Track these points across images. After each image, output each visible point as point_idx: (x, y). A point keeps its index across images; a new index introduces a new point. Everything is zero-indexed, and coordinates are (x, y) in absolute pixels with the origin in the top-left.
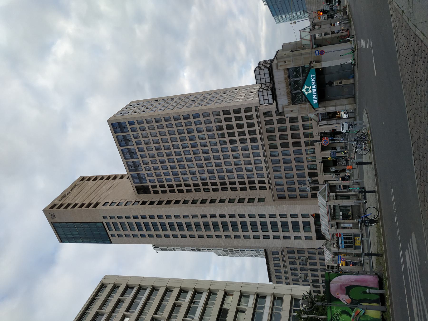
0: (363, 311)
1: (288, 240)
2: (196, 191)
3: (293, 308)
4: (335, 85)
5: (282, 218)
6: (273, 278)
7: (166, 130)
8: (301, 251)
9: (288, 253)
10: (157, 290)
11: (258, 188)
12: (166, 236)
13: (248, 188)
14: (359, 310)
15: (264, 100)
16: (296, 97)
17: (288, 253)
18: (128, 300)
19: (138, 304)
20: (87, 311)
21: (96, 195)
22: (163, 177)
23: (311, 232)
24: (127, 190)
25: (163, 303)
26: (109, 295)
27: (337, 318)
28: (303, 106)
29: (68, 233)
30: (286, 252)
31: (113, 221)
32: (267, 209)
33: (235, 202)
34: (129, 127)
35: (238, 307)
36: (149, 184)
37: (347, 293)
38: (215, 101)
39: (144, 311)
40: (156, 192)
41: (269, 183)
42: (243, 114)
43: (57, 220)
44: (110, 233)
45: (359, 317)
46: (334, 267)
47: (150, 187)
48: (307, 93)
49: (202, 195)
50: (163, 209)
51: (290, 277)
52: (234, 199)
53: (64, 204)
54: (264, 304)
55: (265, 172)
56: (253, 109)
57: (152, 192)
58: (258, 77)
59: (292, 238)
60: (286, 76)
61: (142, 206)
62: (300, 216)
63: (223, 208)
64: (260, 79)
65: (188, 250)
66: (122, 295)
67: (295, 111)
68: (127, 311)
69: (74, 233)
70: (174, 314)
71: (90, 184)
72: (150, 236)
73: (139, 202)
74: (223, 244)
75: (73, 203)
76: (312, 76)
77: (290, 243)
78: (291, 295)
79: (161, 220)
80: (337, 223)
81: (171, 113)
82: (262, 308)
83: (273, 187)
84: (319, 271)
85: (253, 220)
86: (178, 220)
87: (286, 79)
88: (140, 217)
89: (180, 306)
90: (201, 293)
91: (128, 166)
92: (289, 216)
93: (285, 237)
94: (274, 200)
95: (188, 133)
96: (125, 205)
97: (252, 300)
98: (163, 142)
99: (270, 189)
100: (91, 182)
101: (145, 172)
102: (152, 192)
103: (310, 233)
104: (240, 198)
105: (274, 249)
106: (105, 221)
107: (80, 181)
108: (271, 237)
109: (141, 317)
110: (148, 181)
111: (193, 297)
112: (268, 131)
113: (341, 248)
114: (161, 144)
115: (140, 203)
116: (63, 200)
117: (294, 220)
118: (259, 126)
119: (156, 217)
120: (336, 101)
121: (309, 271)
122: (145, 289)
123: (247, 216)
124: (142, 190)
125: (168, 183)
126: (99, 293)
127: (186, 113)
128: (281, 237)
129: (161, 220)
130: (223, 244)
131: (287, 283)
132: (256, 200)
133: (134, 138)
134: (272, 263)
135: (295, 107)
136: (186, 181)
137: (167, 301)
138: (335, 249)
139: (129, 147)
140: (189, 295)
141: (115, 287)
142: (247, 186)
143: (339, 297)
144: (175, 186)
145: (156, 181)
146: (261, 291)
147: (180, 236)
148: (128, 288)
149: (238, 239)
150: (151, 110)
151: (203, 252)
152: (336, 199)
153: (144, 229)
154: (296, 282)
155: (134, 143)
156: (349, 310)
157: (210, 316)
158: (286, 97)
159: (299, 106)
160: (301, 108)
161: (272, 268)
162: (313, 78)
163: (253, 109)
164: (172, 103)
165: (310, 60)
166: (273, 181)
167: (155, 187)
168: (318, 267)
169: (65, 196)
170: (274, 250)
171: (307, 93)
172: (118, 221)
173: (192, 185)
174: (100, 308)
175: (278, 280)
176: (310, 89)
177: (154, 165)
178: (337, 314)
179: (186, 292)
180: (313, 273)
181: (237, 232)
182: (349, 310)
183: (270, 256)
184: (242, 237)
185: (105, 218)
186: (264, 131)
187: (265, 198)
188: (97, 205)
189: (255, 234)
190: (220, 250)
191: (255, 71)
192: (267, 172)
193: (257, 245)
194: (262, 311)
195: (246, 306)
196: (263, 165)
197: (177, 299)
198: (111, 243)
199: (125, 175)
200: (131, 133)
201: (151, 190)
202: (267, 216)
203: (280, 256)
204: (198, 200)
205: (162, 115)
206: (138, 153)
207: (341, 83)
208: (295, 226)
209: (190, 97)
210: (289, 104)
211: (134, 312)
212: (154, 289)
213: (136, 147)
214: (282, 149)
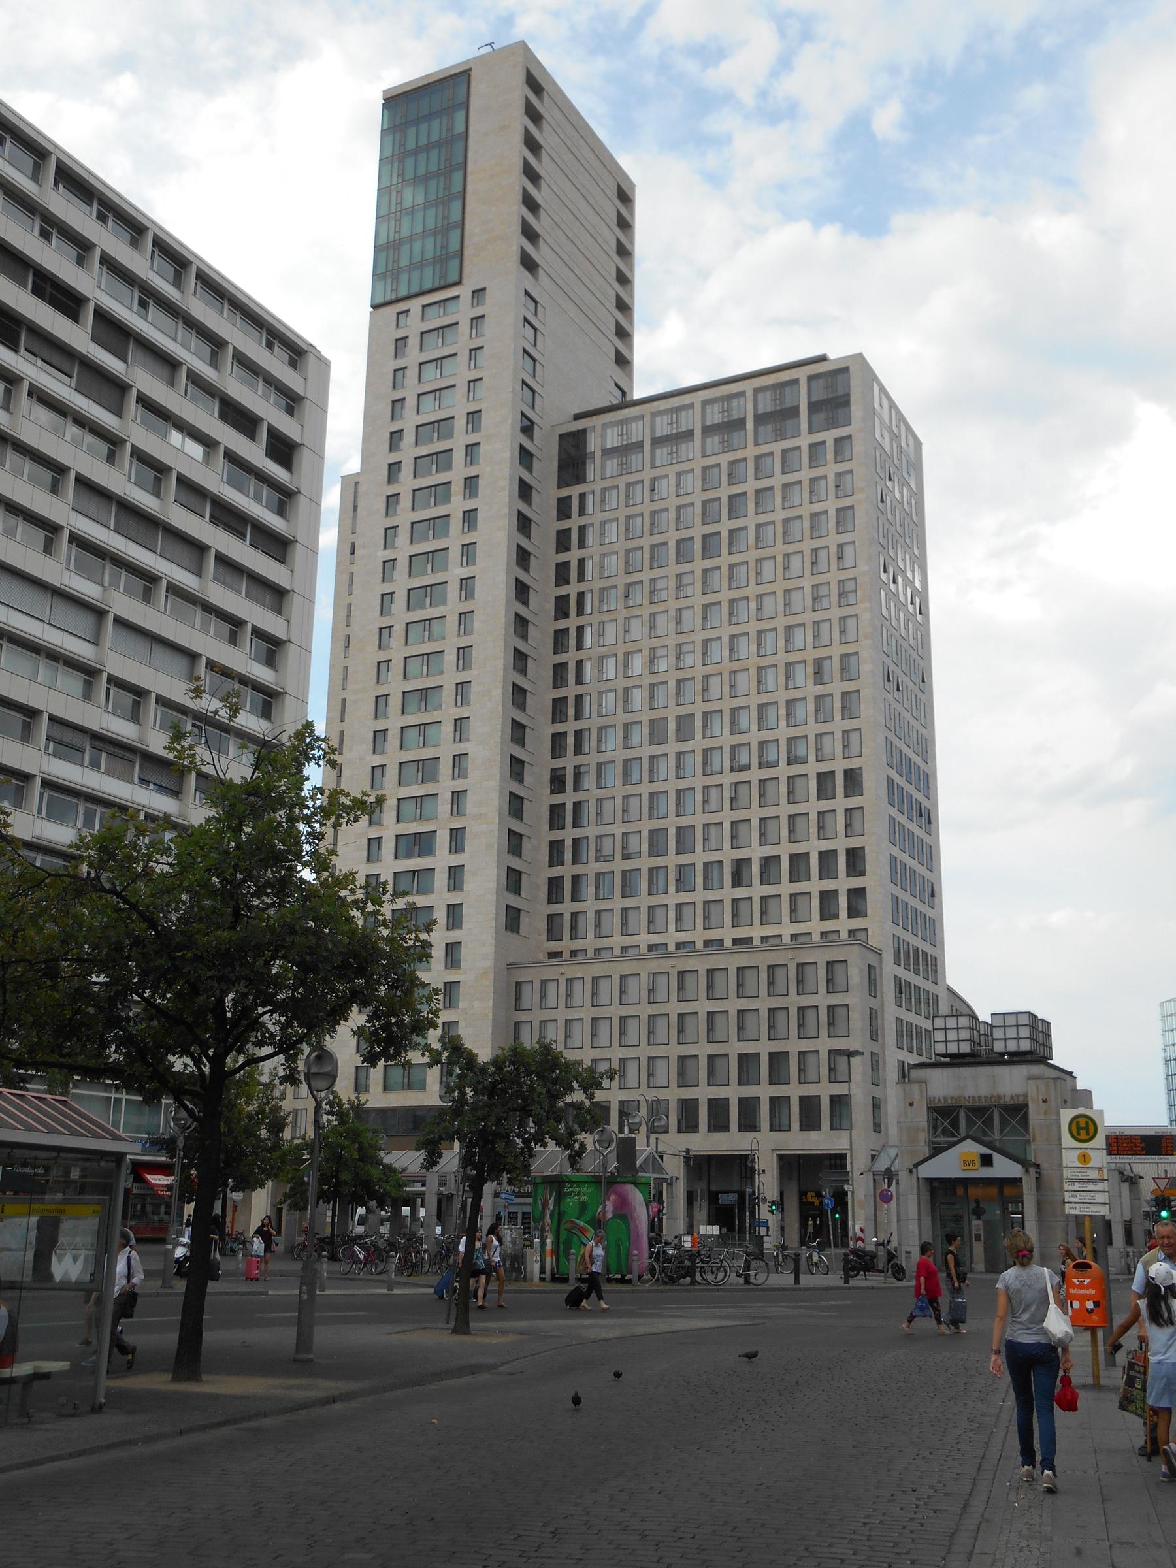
4: (974, 1222)
15: (946, 1029)
16: (948, 1121)
19: (239, 488)
21: (566, 258)
28: (923, 1136)
34: (829, 436)
44: (415, 305)
57: (565, 492)
58: (1011, 1021)
60: (1008, 1099)
71: (605, 230)
75: (543, 167)
83: (563, 969)
88: (472, 439)
94: (511, 967)
102: (565, 492)
103: (380, 1088)
104: (525, 840)
107: (620, 189)
123: (455, 860)
132: (514, 901)
133: (785, 452)
139: (750, 425)
140: (262, 674)
141: (292, 402)
155: (765, 449)
156: (588, 1216)
158: (956, 1094)
163: (856, 923)
165: (1045, 1166)
178: (579, 1194)
185: (478, 293)
191: (1029, 1013)
195: (40, 812)
198: (375, 307)
200: (804, 441)
201: (574, 491)
207: (978, 1238)
209: (918, 680)
210: (930, 1100)
213: (751, 452)
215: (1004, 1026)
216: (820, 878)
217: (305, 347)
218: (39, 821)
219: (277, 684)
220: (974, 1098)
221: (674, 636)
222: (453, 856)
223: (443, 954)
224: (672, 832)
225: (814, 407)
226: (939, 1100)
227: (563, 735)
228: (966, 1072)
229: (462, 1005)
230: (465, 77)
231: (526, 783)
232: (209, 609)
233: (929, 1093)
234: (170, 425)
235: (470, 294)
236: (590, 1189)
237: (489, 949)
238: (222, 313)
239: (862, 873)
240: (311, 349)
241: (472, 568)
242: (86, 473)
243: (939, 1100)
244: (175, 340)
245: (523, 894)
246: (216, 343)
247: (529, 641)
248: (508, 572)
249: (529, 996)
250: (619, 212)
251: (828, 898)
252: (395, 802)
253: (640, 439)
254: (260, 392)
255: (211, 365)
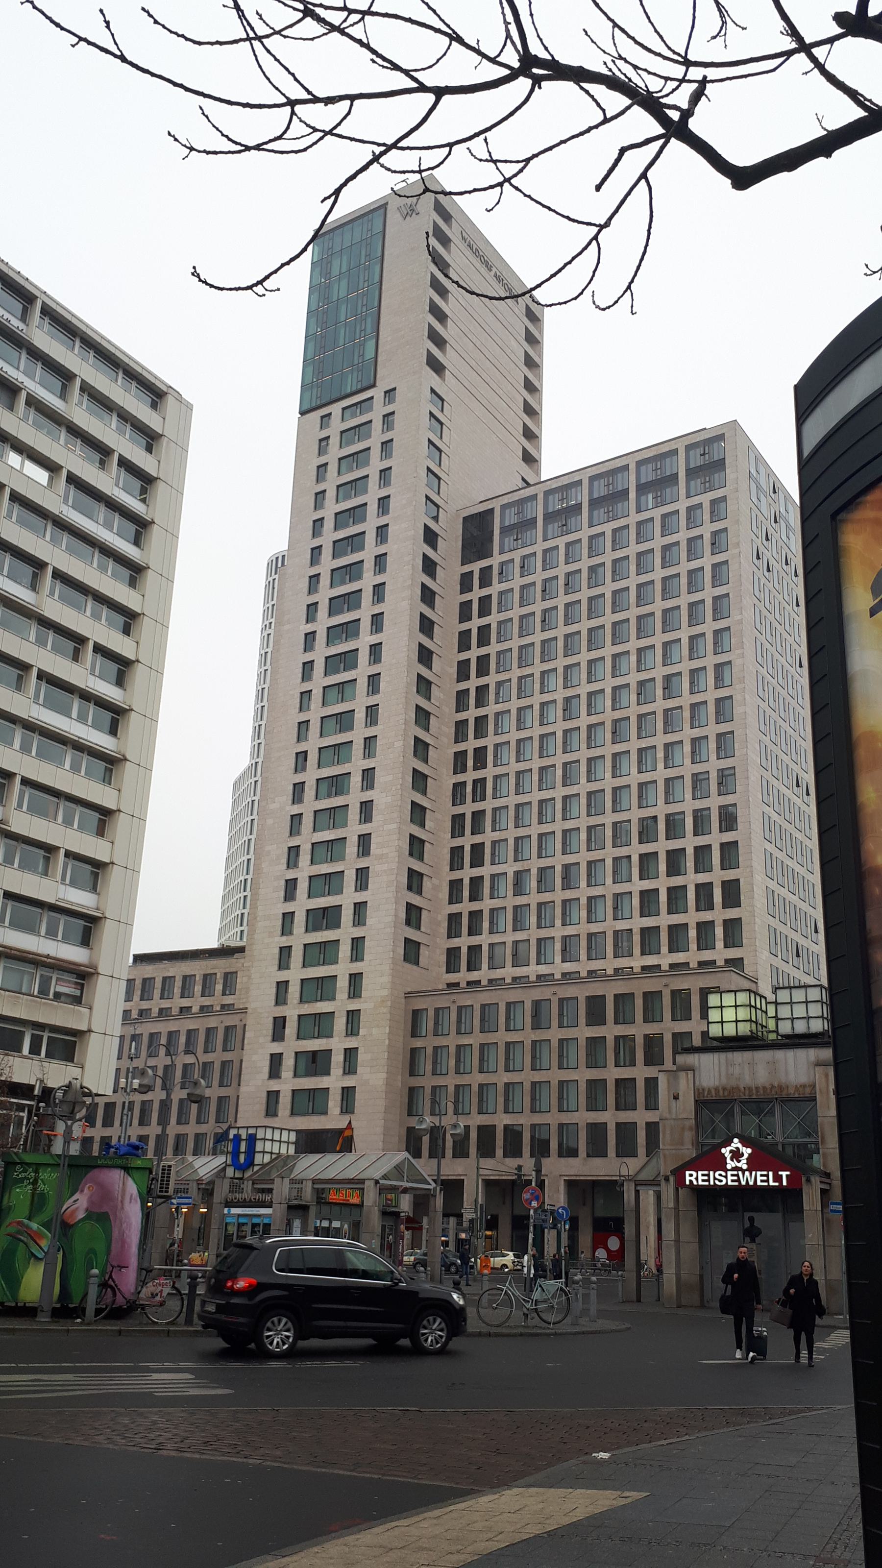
0: (40, 1255)
1: (270, 1032)
2: (461, 726)
3: (46, 1035)
5: (344, 1019)
6: (149, 970)
7: (684, 634)
8: (230, 1073)
9: (227, 1028)
10: (133, 583)
11: (455, 942)
12: (312, 608)
13: (455, 908)
14: (44, 1244)
16: (717, 1114)
17: (227, 1028)
18: (107, 481)
20: (78, 343)
21: (473, 363)
22: (515, 613)
23: (292, 1113)
24: (479, 478)
25: (90, 603)
26: (124, 417)
27: (26, 1178)
28: (688, 1136)
29: (345, 258)
30: (230, 1021)
31: (377, 425)
32: (380, 969)
33: (411, 859)
35: (62, 852)
36: (495, 561)
37: (90, 1215)
38: (775, 816)
39: (66, 538)
40: (466, 582)
41: (468, 983)
42: (718, 915)
43: (393, 217)
44: (336, 409)
45: (25, 1240)
46: (165, 1186)
47: (484, 563)
48: (728, 1156)
49: (444, 748)
50: (405, 604)
51: (145, 1029)
52: (421, 858)
53: (449, 252)
54: (66, 939)
55: (508, 972)
56: (733, 953)
57: (467, 568)
59: (276, 1048)
60: (791, 1091)
61: (422, 532)
62: (349, 1082)
63: (395, 815)
64: (737, 1021)
65: (263, 675)
66: (124, 463)
67: (676, 1108)
68: (73, 480)
69: (344, 284)
70: (51, 636)
71: (514, 343)
72: (316, 551)
73: (436, 519)
74: (273, 806)
76: (784, 1174)
77: (261, 1040)
78: (90, 1031)
79: (367, 597)
80: (304, 1208)
81: (743, 656)
82: (51, 933)
83: (454, 997)
84: (163, 1095)
85: (347, 915)
86: (363, 657)
87: (781, 1087)
88: (382, 521)
89: (76, 657)
90: (113, 731)
91: (567, 486)
92: (351, 1043)
93: (279, 1024)
94: (409, 995)
95: (666, 711)
96: (428, 469)
97: (79, 898)
98: (639, 618)
99: (449, 985)
100: (519, 348)
101: (539, 547)
102: (467, 568)
103: (288, 1112)
104: (425, 879)
105: (245, 979)
106: (377, 393)
108: (283, 976)
109: (24, 355)
110: (505, 557)
111: (102, 703)
112: (651, 998)
113: (226, 1211)
114: (633, 613)
115: (432, 525)
116: (462, 246)
117: (337, 1059)
118: (671, 965)
119: (379, 579)
120: (696, 1246)
121: (159, 1130)
122: (137, 542)
123: (360, 897)
124: (477, 533)
125: (494, 627)
126: (134, 384)
127: (738, 710)
128: (281, 1008)
129: (367, 597)
130: (273, 806)
131: (126, 1013)
134: (197, 968)
135: (686, 1107)
136: (497, 694)
137: (96, 616)
138: (222, 1192)
139: (632, 495)
141: (150, 439)
142: (465, 907)
143: (82, 1191)
144: (483, 651)
145: (504, 586)
146: (107, 932)
147: (308, 657)
148: (146, 482)
149: (284, 861)
150: (763, 580)
151: (251, 729)
152: (385, 1214)
153: (341, 534)
154: (129, 1044)
156: (45, 1216)
157: (40, 755)
159: (687, 1123)
160: (683, 1129)
161: (177, 970)
162: (778, 1178)
163: (733, 953)
164: (783, 660)
166: (475, 1000)
167: (485, 581)
168: (173, 1129)
169: (476, 253)
170: (241, 979)
171: (728, 1156)
172: (374, 441)
173: (481, 712)
174: (87, 389)
175: (138, 984)
176: (737, 1168)
177: (561, 581)
179: (120, 682)
180: (156, 1106)
181: (309, 857)
182: (45, 1216)
183: (219, 966)
184: (291, 875)
185: (390, 393)
186: (651, 985)
187: (417, 963)
188: (437, 367)
189: (300, 920)
190: (252, 789)
192: (508, 980)
193: (260, 924)
194: (43, 931)
195: (63, 878)
196: (532, 970)
197: (99, 649)
198: (302, 413)
199: (538, 473)
200: (682, 505)
201: (476, 567)
202: (356, 967)
203: (216, 1000)
204: (427, 729)
205: (740, 622)
206: (608, 528)
208: (316, 1063)
211: (66, 501)
212: (135, 572)
213: (634, 518)
214: (582, 1043)
215: (791, 1003)
216: (697, 910)
217: (165, 389)
218: (63, 887)
219: (124, 703)
220: (750, 1089)
221: (562, 690)
222: (358, 894)
223: (347, 984)
224: (558, 869)
225: (691, 473)
226: (709, 1091)
227: (464, 784)
228: (738, 1057)
229: (362, 1032)
230: (382, 210)
231: (427, 828)
232: (46, 623)
233: (697, 1083)
234: (7, 447)
235: (383, 394)
236: (54, 1176)
237: (386, 979)
238: (117, 381)
239: (738, 905)
240: (170, 391)
241: (379, 635)
242: (64, 568)
243: (709, 1091)
244: (18, 369)
245: (422, 929)
246: (65, 376)
247: (432, 701)
248: (410, 636)
249: (427, 1024)
250: (526, 328)
251: (705, 928)
252: (310, 846)
253: (534, 516)
254: (127, 436)
255: (60, 397)
